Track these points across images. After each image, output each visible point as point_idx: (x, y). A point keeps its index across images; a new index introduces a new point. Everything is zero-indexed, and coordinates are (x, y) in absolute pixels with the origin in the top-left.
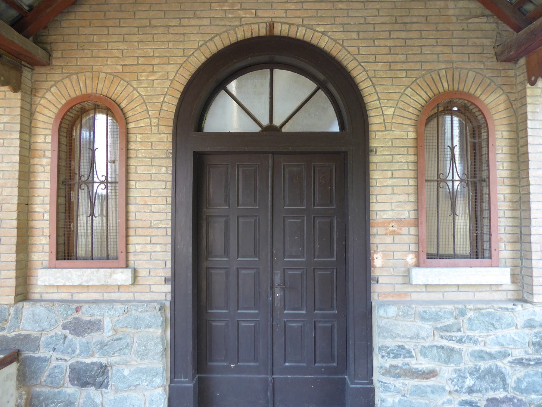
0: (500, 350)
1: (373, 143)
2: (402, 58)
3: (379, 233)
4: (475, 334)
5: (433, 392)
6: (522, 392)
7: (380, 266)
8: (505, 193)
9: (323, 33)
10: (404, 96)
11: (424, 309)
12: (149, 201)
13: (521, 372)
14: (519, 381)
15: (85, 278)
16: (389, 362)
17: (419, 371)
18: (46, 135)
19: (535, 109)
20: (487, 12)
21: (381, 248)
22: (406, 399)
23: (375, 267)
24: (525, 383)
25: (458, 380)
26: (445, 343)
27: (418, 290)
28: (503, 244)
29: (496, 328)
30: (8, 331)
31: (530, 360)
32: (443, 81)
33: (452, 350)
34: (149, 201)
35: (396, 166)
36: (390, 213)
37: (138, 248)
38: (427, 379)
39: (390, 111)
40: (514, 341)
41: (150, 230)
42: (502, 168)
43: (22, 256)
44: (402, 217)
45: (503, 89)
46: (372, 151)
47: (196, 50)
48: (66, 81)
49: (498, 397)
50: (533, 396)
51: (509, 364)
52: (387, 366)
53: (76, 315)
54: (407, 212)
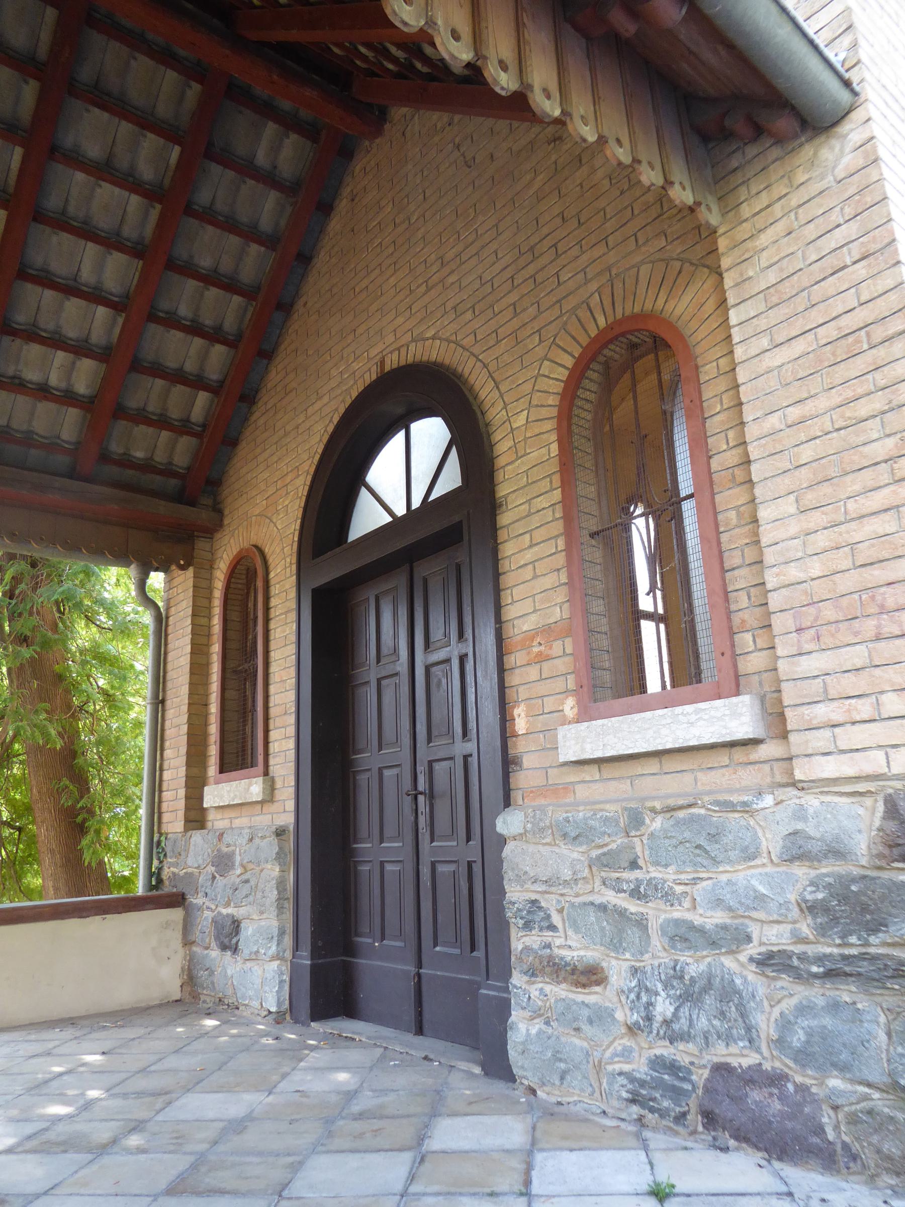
0: (728, 921)
1: (502, 491)
2: (532, 311)
3: (518, 664)
4: (668, 875)
5: (590, 1022)
6: (803, 1057)
7: (524, 732)
8: (740, 503)
9: (433, 338)
10: (540, 379)
11: (565, 815)
13: (794, 994)
14: (785, 1024)
17: (567, 964)
19: (741, 274)
21: (523, 693)
22: (550, 1031)
23: (516, 736)
24: (801, 1032)
25: (638, 997)
26: (610, 897)
27: (588, 778)
28: (748, 637)
29: (715, 861)
32: (597, 316)
33: (622, 913)
35: (536, 521)
36: (533, 618)
38: (584, 986)
39: (520, 421)
40: (761, 898)
42: (725, 447)
43: (195, 771)
44: (552, 620)
45: (708, 263)
46: (501, 505)
49: (734, 1062)
50: (835, 1082)
51: (753, 967)
54: (558, 611)
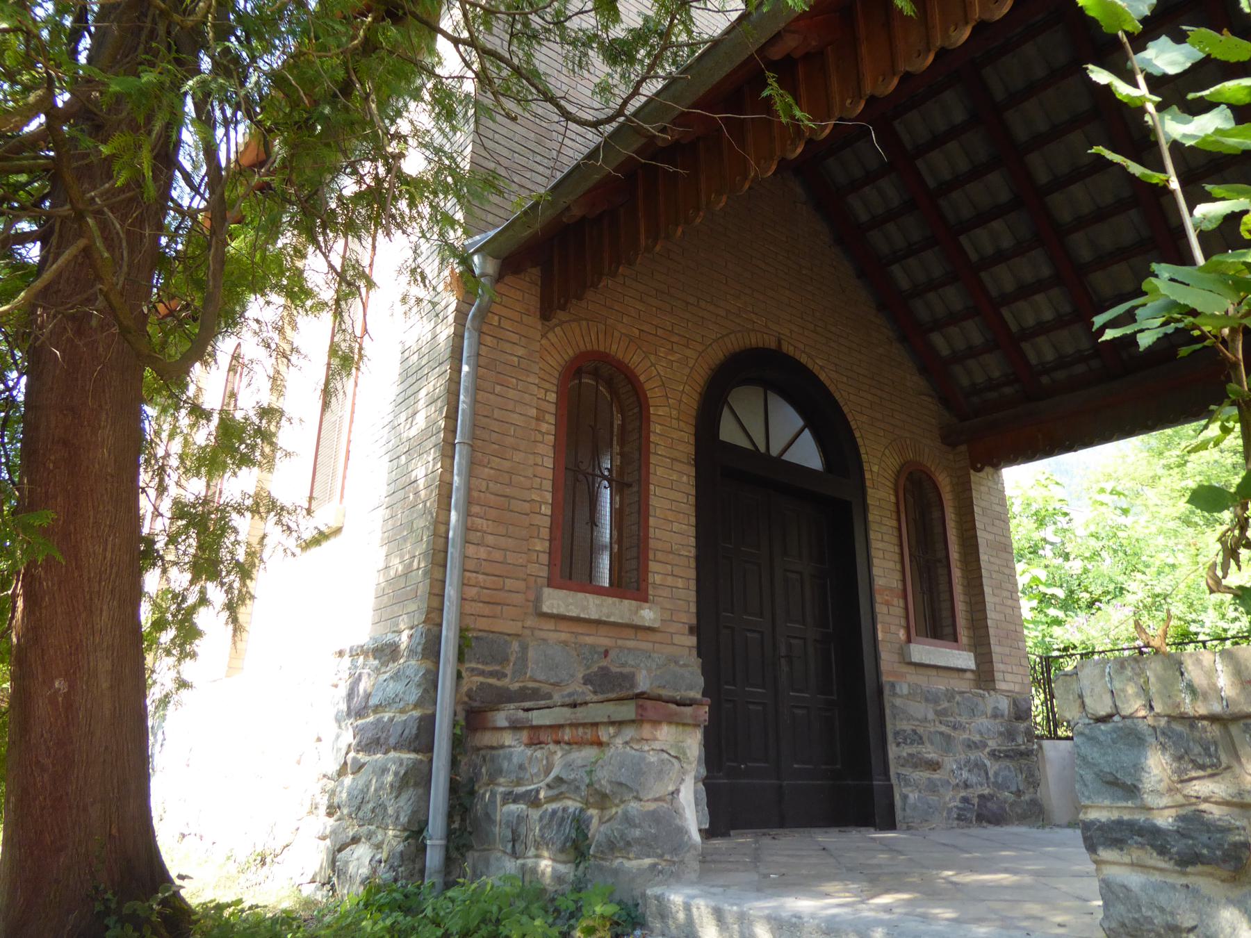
12: (670, 516)
15: (605, 610)
16: (906, 751)
18: (547, 391)
20: (1204, 422)
30: (512, 679)
31: (1000, 751)
34: (670, 516)
37: (658, 579)
41: (671, 556)
47: (715, 341)
48: (574, 325)
52: (905, 754)
53: (604, 663)
